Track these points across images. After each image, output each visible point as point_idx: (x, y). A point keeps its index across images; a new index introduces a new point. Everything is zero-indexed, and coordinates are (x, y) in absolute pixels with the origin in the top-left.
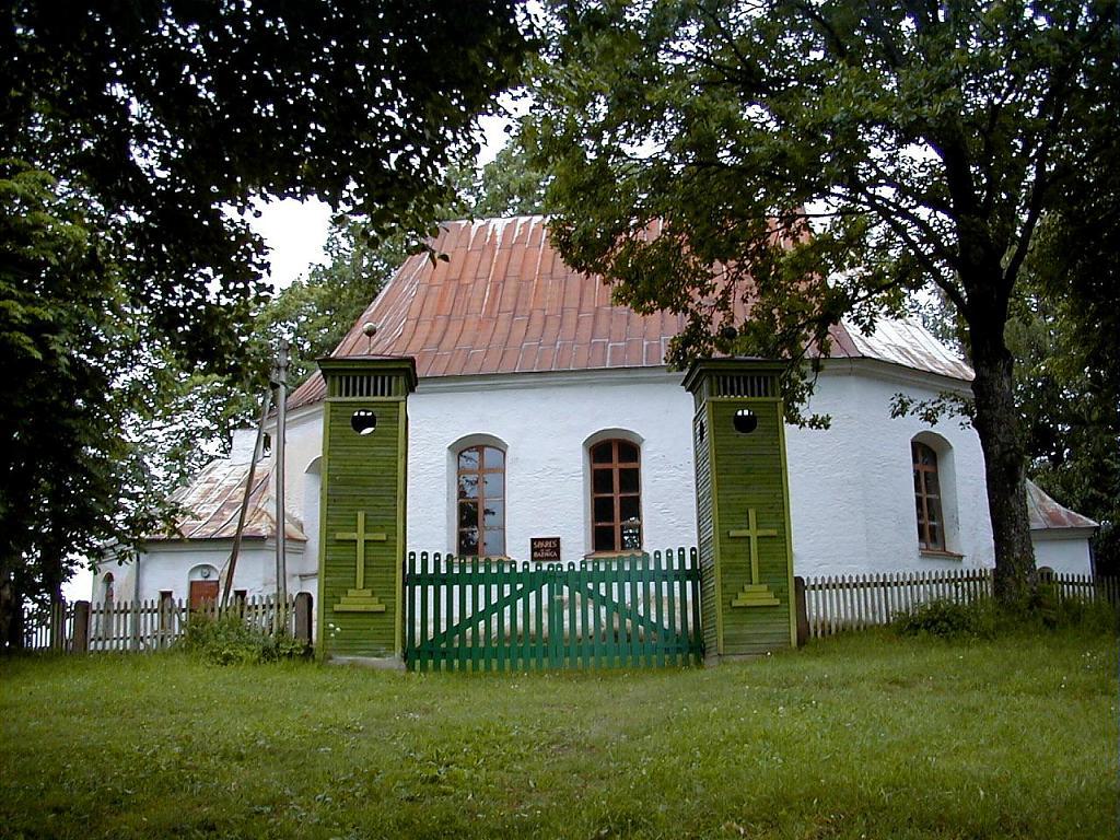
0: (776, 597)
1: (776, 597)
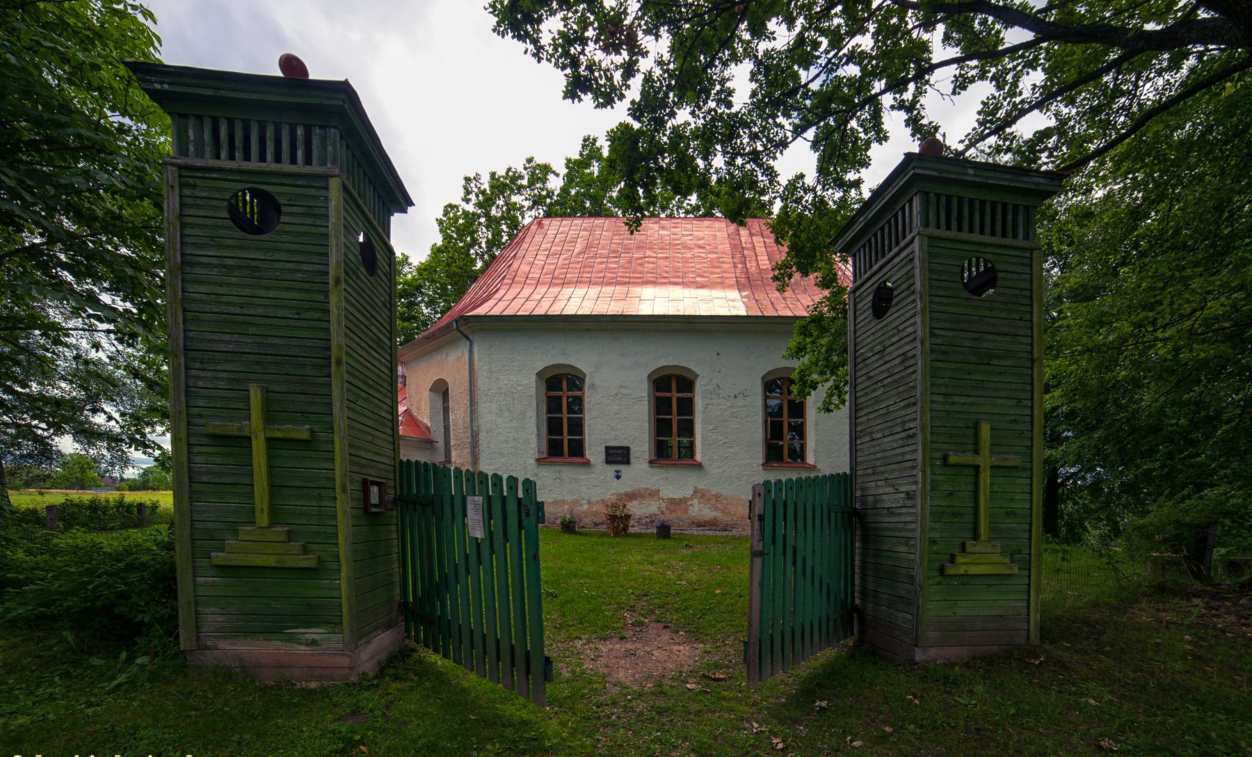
0: (1012, 562)
1: (1012, 562)
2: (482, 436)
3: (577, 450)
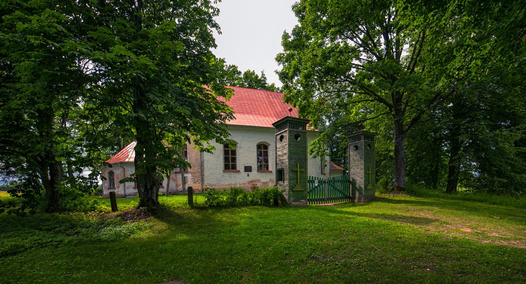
2: (205, 163)
3: (234, 167)
